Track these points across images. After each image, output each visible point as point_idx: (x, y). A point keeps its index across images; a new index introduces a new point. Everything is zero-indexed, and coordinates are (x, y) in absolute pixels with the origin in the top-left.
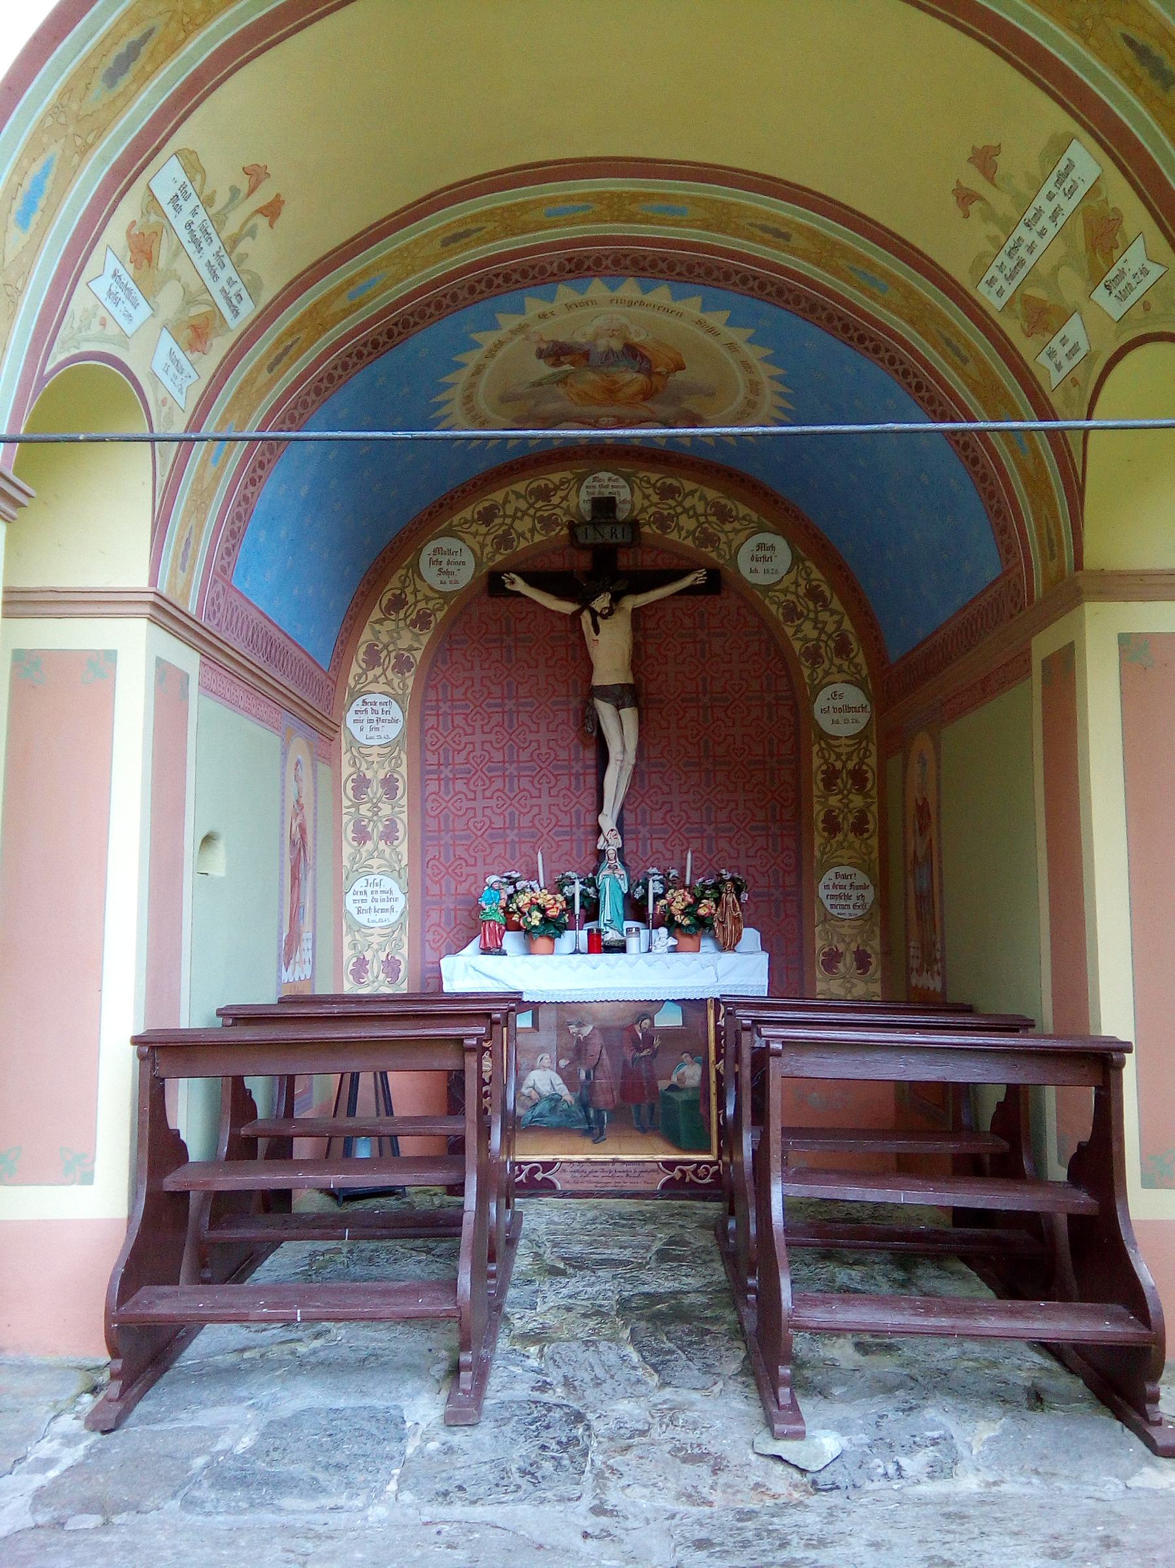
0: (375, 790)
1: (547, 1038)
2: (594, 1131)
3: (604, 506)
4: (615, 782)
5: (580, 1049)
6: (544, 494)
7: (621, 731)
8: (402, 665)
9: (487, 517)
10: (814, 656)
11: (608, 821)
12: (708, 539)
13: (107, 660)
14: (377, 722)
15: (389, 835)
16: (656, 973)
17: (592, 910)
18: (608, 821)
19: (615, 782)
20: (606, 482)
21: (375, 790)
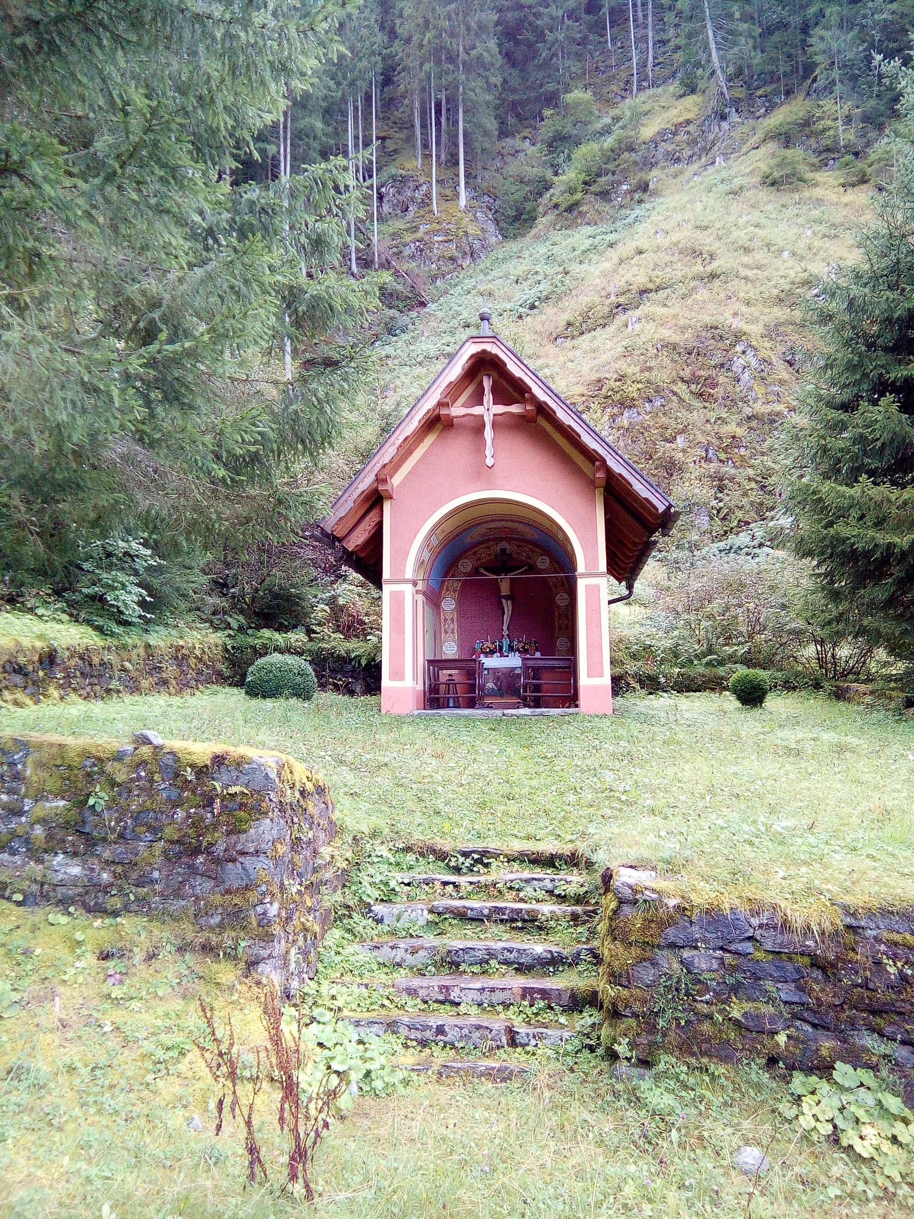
0: (449, 622)
1: (491, 676)
2: (501, 696)
3: (503, 550)
4: (506, 618)
5: (498, 678)
6: (489, 548)
7: (508, 606)
8: (454, 591)
9: (475, 553)
10: (556, 586)
11: (505, 628)
12: (530, 558)
13: (403, 593)
14: (449, 605)
15: (453, 632)
16: (514, 661)
17: (501, 648)
18: (505, 628)
19: (506, 618)
20: (504, 545)
21: (449, 622)
